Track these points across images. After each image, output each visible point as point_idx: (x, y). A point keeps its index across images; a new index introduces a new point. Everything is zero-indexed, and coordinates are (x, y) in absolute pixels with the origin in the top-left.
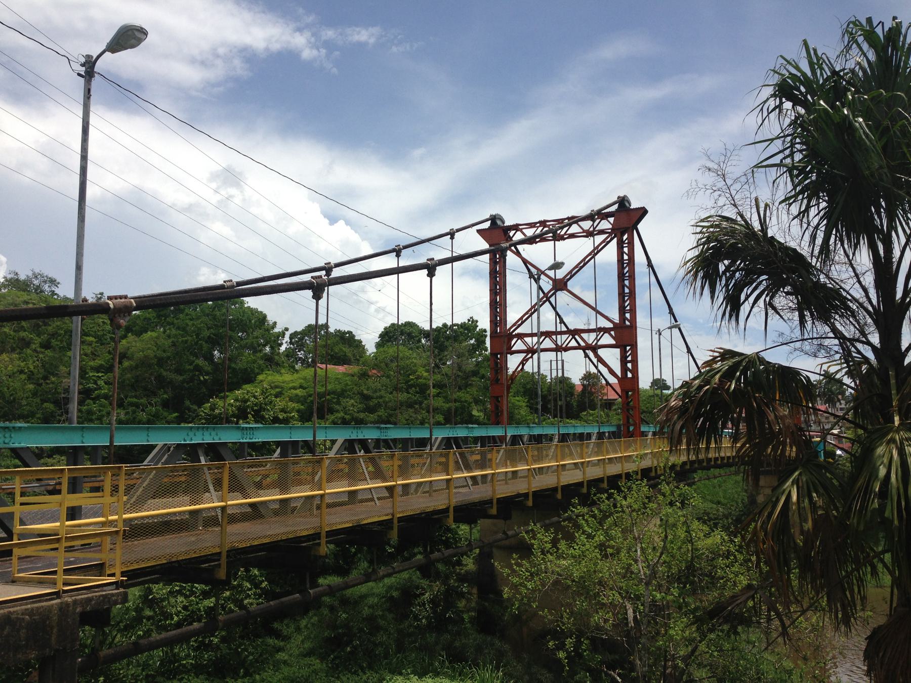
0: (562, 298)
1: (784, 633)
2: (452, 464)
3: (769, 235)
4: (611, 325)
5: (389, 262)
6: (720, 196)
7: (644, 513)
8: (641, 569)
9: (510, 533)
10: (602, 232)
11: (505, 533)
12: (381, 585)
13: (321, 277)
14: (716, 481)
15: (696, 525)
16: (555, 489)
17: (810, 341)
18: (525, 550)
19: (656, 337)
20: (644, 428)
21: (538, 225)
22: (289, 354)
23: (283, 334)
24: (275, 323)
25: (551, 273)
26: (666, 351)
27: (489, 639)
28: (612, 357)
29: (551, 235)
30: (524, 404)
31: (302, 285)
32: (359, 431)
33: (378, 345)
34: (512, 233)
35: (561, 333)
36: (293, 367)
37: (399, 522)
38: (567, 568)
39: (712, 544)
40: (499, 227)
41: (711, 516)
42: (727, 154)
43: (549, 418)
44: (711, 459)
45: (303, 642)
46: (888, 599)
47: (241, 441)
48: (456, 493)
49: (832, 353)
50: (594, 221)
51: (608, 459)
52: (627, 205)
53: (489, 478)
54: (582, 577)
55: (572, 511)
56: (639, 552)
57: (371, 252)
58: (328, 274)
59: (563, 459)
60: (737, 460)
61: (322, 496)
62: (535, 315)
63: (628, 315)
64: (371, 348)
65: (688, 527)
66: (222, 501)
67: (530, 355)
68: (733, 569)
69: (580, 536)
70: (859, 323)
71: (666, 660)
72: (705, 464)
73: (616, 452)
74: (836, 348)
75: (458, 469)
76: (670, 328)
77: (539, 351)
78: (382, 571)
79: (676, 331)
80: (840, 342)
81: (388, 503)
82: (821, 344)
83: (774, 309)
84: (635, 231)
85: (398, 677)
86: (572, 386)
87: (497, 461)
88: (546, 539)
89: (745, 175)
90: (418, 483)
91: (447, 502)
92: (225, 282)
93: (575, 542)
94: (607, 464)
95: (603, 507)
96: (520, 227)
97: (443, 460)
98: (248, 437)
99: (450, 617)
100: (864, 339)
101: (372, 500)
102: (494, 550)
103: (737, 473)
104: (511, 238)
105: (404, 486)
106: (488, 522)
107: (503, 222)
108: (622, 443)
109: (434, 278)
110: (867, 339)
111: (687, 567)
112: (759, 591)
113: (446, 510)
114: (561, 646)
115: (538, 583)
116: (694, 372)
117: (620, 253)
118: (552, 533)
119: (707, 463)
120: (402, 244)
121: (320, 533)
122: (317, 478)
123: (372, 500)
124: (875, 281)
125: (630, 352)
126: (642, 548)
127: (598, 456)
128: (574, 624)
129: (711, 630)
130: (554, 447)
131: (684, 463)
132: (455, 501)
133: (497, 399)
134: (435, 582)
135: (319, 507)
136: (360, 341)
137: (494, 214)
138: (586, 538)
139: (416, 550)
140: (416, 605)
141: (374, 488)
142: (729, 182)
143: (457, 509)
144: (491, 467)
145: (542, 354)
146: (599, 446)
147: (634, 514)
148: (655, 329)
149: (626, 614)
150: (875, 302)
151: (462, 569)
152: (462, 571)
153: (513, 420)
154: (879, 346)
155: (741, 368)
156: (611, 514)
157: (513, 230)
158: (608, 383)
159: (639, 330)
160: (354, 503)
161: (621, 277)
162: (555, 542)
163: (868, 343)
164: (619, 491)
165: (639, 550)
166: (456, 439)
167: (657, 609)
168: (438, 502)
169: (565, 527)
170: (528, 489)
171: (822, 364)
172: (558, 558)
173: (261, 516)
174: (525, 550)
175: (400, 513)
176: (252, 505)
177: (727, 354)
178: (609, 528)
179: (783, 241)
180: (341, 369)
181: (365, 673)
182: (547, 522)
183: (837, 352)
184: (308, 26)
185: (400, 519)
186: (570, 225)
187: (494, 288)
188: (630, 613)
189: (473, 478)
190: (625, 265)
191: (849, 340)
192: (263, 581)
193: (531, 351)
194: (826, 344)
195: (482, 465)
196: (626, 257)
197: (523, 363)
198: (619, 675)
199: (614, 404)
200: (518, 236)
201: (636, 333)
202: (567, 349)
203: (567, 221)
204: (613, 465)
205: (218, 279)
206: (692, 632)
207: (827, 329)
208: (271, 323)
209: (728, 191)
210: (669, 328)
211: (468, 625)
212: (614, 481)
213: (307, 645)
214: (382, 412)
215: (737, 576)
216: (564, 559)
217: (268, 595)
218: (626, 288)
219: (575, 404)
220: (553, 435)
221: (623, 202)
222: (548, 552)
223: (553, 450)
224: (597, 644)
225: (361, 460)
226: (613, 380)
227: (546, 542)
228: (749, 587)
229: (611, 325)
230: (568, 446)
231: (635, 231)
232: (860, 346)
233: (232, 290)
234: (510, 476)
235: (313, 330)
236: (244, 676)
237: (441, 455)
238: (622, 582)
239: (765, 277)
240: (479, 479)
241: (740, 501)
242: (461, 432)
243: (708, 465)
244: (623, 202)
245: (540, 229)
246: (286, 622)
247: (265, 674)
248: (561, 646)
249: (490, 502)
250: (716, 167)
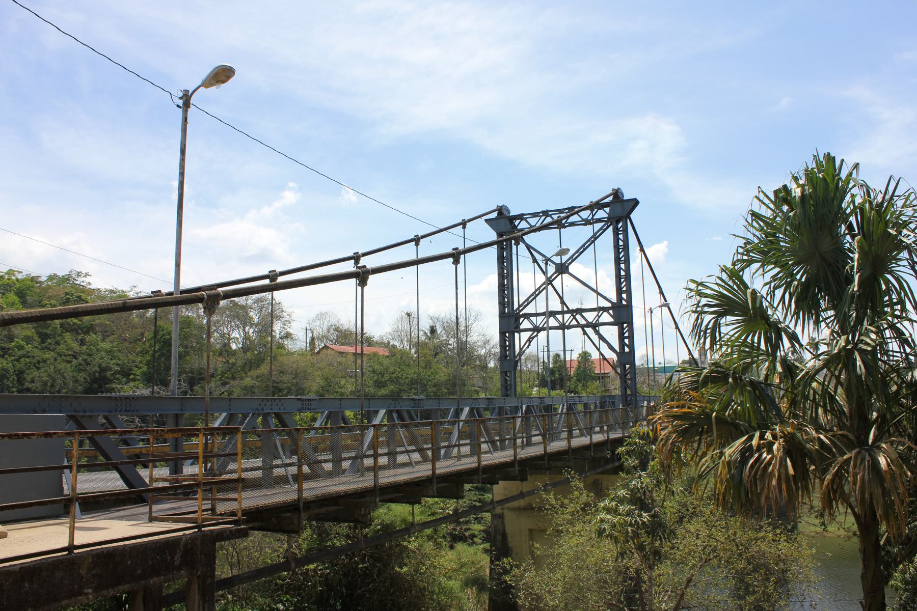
4: (609, 305)
5: (407, 253)
10: (599, 220)
21: (541, 214)
28: (611, 333)
34: (517, 223)
52: (621, 196)
63: (624, 296)
76: (661, 307)
79: (665, 309)
84: (773, 266)
92: (270, 272)
96: (525, 217)
117: (616, 240)
196: (621, 243)
210: (659, 307)
221: (617, 194)
231: (773, 266)
244: (617, 194)
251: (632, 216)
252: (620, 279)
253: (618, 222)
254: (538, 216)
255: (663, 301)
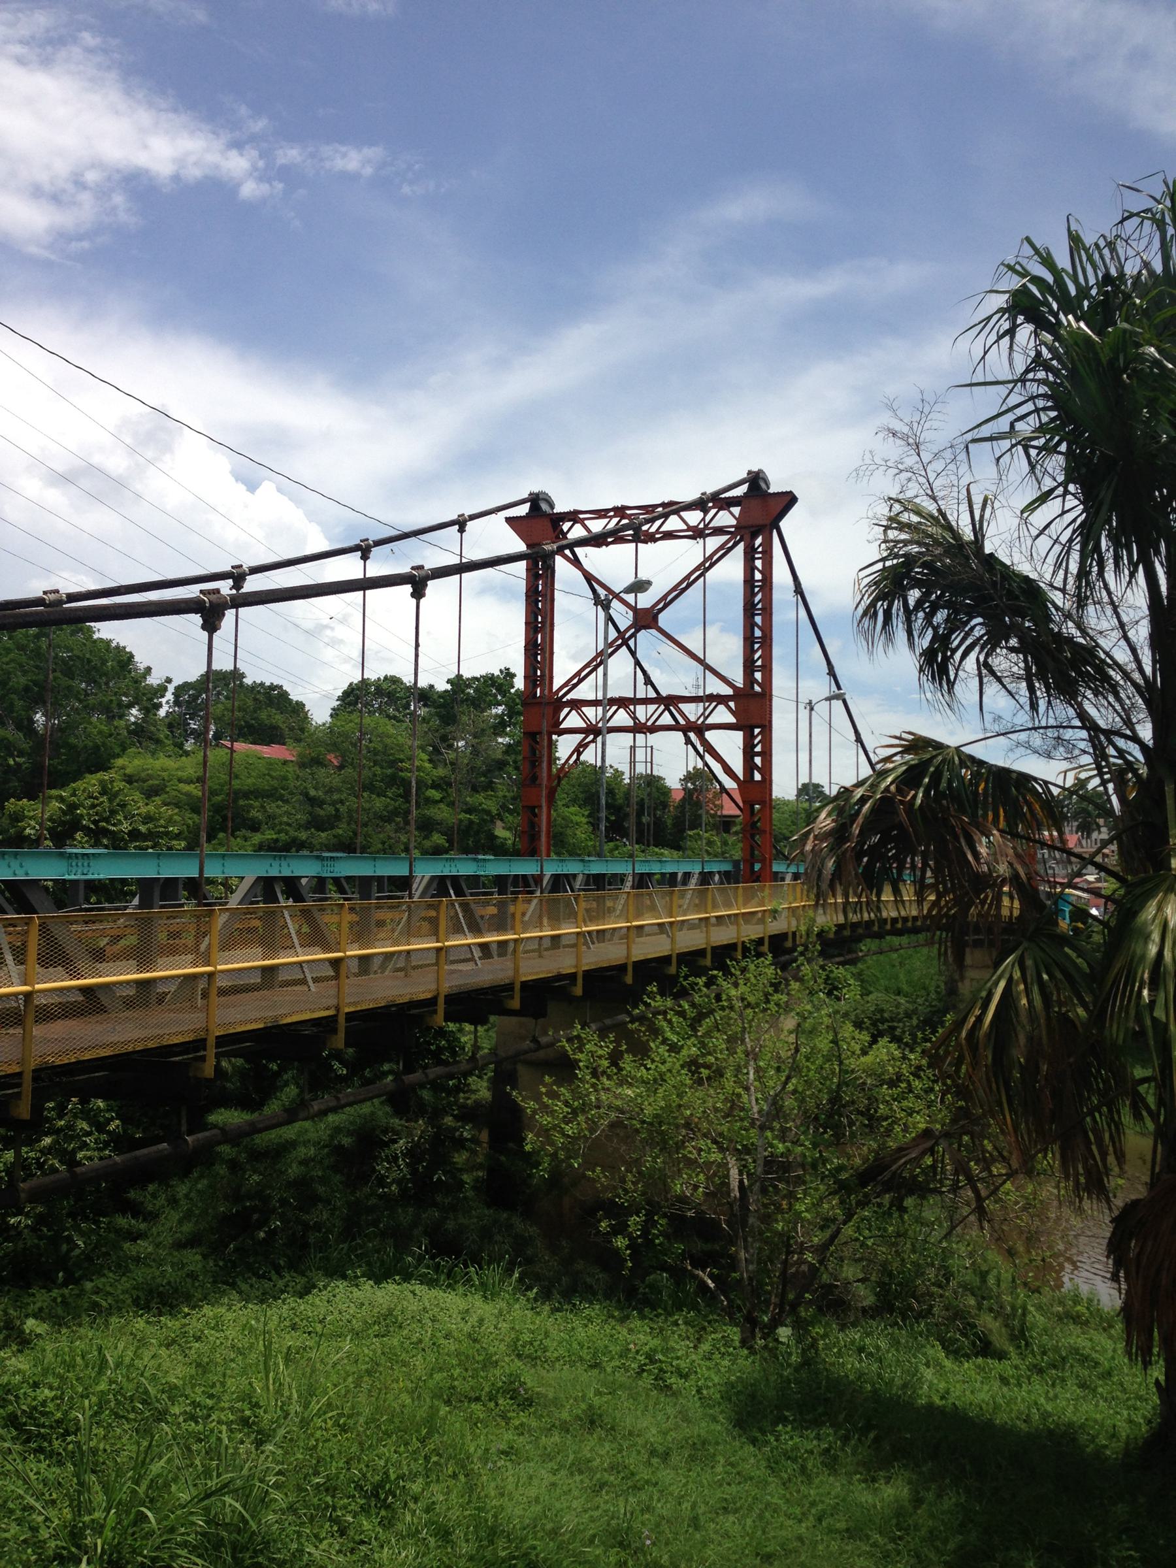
0: (646, 640)
1: (981, 1211)
2: (443, 924)
3: (987, 551)
4: (729, 691)
5: (348, 568)
6: (909, 480)
7: (765, 1010)
8: (754, 1104)
9: (544, 1040)
10: (719, 531)
11: (535, 1040)
12: (323, 1126)
13: (217, 591)
14: (895, 956)
15: (848, 1029)
16: (622, 968)
17: (1041, 731)
18: (564, 1068)
19: (804, 714)
20: (777, 867)
21: (612, 514)
22: (175, 724)
23: (162, 690)
24: (148, 670)
25: (630, 598)
26: (820, 738)
27: (505, 1215)
28: (730, 745)
29: (631, 532)
30: (584, 820)
31: (183, 605)
32: (284, 863)
33: (335, 712)
34: (566, 526)
35: (646, 701)
36: (181, 746)
37: (218, 1045)
38: (632, 1100)
39: (873, 1063)
40: (545, 515)
41: (886, 1015)
42: (925, 406)
43: (625, 845)
44: (885, 920)
45: (180, 1222)
46: (1149, 1158)
47: (67, 877)
48: (453, 972)
49: (1077, 752)
50: (706, 511)
51: (717, 917)
52: (763, 486)
53: (511, 946)
54: (656, 1116)
55: (646, 1004)
56: (751, 1076)
57: (325, 547)
58: (238, 585)
59: (638, 916)
60: (928, 922)
61: (211, 975)
62: (601, 670)
63: (758, 676)
64: (320, 714)
65: (836, 1034)
66: (25, 984)
67: (591, 737)
68: (905, 1103)
69: (658, 1047)
70: (1122, 704)
71: (789, 1253)
72: (876, 928)
73: (728, 905)
74: (1083, 745)
75: (457, 930)
76: (829, 699)
77: (605, 731)
78: (328, 1099)
79: (838, 705)
80: (1090, 735)
81: (330, 988)
82: (1059, 738)
83: (992, 673)
84: (775, 533)
85: (338, 1283)
86: (666, 792)
87: (526, 918)
88: (600, 1052)
89: (951, 447)
90: (386, 954)
91: (433, 987)
92: (45, 593)
93: (649, 1057)
94: (714, 925)
95: (697, 999)
96: (581, 516)
97: (433, 913)
98: (80, 871)
99: (439, 1179)
100: (1128, 732)
101: (303, 982)
102: (522, 1070)
103: (929, 943)
104: (565, 535)
105: (362, 958)
106: (506, 1020)
107: (552, 506)
108: (740, 891)
109: (422, 601)
110: (1133, 730)
111: (830, 1101)
112: (941, 1141)
113: (432, 1002)
114: (620, 1229)
115: (584, 1126)
116: (866, 771)
117: (749, 569)
118: (611, 1042)
119: (880, 927)
120: (373, 537)
121: (205, 1040)
122: (203, 947)
123: (303, 982)
124: (1151, 635)
125: (759, 738)
126: (758, 1070)
127: (698, 912)
128: (643, 1194)
129: (862, 1204)
130: (625, 896)
131: (840, 927)
132: (446, 987)
133: (532, 811)
134: (416, 1121)
135: (205, 995)
136: (300, 705)
137: (536, 491)
138: (668, 1051)
139: (386, 1067)
140: (383, 1160)
141: (308, 962)
142: (927, 458)
143: (451, 999)
144: (513, 929)
145: (611, 737)
146: (702, 894)
147: (749, 1011)
148: (803, 699)
149: (727, 1176)
150: (1148, 670)
151: (468, 1098)
152: (469, 1102)
153: (561, 845)
154: (1151, 743)
155: (932, 769)
156: (712, 1012)
157: (569, 520)
158: (723, 789)
159: (775, 701)
160: (270, 987)
161: (749, 609)
162: (615, 1058)
163: (1135, 739)
164: (727, 972)
165: (752, 1073)
166: (455, 880)
167: (777, 1167)
168: (419, 988)
169: (632, 1032)
170: (576, 966)
171: (1065, 772)
172: (620, 1084)
173: (102, 1010)
174: (564, 1068)
175: (350, 1004)
176: (86, 990)
177: (916, 744)
178: (708, 1034)
179: (1008, 563)
180: (266, 751)
181: (282, 1277)
182: (608, 1022)
183: (1085, 752)
184: (253, 139)
185: (350, 1016)
186: (666, 516)
187: (532, 620)
188: (734, 1173)
189: (484, 947)
190: (756, 590)
191: (1104, 732)
192: (112, 1119)
193: (593, 731)
194: (1067, 737)
195: (500, 924)
196: (758, 576)
197: (579, 749)
198: (711, 1276)
199: (734, 823)
200: (577, 532)
201: (771, 706)
202: (654, 729)
203: (660, 509)
204: (724, 928)
205: (33, 588)
206: (832, 1207)
207: (1071, 712)
208: (142, 666)
209: (923, 473)
210: (826, 699)
211: (470, 1194)
212: (723, 955)
213: (187, 1228)
214: (342, 830)
215: (910, 1115)
216: (630, 1085)
217: (120, 1142)
218: (756, 629)
219: (669, 822)
220: (625, 875)
221: (756, 480)
222: (604, 1073)
223: (622, 902)
224: (680, 1226)
225: (286, 914)
226: (730, 784)
227: (600, 1057)
228: (927, 1133)
229: (730, 692)
230: (650, 895)
231: (775, 533)
232: (1121, 743)
233: (58, 609)
234: (547, 943)
235: (212, 679)
236: (65, 1284)
237: (430, 906)
238: (721, 1124)
239: (980, 620)
240: (494, 947)
241: (932, 989)
242: (464, 868)
243: (879, 930)
244: (756, 480)
245: (615, 520)
246: (151, 1188)
247: (103, 1280)
248: (620, 1229)
249: (508, 988)
250: (906, 430)
251: (783, 524)
252: (753, 643)
253: (754, 536)
254: (605, 517)
255: (834, 687)
